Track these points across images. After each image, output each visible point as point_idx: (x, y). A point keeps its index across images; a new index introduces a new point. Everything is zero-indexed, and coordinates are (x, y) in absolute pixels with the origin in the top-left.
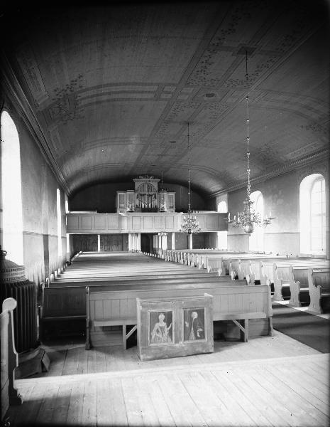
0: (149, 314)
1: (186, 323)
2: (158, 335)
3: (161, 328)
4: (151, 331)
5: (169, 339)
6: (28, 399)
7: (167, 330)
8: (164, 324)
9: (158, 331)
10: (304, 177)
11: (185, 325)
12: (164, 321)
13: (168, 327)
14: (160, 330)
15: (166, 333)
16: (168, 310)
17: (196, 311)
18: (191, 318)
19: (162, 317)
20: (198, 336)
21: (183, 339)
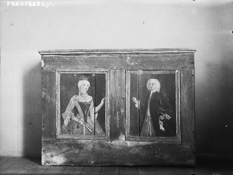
0: (58, 76)
1: (135, 99)
2: (75, 119)
3: (81, 104)
4: (63, 109)
5: (99, 131)
6: (4, 155)
7: (93, 111)
8: (89, 99)
9: (75, 111)
10: (161, 84)
11: (132, 104)
12: (90, 92)
13: (95, 105)
14: (79, 109)
15: (93, 117)
16: (99, 71)
17: (157, 77)
18: (146, 92)
19: (84, 85)
20: (162, 128)
21: (128, 130)
